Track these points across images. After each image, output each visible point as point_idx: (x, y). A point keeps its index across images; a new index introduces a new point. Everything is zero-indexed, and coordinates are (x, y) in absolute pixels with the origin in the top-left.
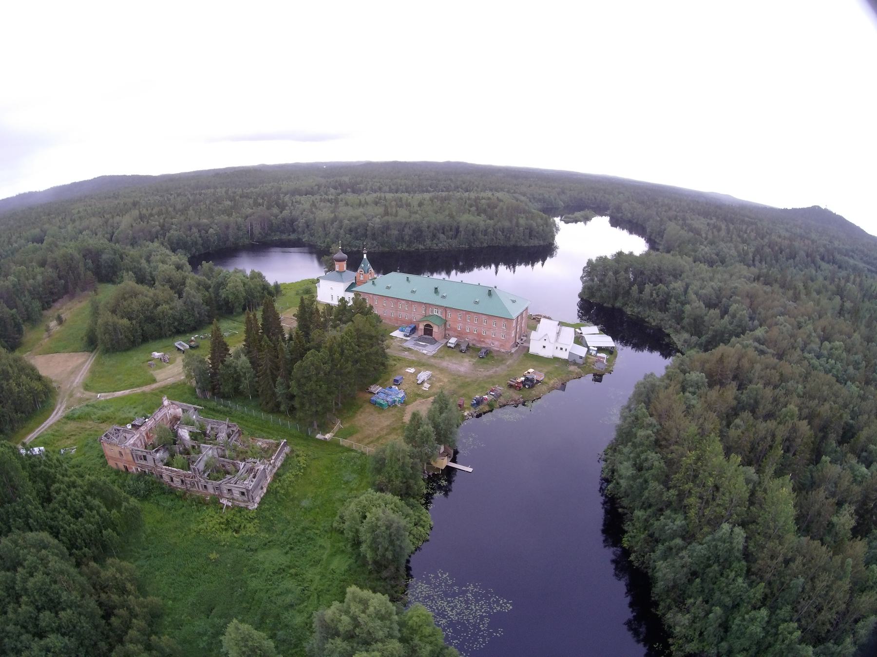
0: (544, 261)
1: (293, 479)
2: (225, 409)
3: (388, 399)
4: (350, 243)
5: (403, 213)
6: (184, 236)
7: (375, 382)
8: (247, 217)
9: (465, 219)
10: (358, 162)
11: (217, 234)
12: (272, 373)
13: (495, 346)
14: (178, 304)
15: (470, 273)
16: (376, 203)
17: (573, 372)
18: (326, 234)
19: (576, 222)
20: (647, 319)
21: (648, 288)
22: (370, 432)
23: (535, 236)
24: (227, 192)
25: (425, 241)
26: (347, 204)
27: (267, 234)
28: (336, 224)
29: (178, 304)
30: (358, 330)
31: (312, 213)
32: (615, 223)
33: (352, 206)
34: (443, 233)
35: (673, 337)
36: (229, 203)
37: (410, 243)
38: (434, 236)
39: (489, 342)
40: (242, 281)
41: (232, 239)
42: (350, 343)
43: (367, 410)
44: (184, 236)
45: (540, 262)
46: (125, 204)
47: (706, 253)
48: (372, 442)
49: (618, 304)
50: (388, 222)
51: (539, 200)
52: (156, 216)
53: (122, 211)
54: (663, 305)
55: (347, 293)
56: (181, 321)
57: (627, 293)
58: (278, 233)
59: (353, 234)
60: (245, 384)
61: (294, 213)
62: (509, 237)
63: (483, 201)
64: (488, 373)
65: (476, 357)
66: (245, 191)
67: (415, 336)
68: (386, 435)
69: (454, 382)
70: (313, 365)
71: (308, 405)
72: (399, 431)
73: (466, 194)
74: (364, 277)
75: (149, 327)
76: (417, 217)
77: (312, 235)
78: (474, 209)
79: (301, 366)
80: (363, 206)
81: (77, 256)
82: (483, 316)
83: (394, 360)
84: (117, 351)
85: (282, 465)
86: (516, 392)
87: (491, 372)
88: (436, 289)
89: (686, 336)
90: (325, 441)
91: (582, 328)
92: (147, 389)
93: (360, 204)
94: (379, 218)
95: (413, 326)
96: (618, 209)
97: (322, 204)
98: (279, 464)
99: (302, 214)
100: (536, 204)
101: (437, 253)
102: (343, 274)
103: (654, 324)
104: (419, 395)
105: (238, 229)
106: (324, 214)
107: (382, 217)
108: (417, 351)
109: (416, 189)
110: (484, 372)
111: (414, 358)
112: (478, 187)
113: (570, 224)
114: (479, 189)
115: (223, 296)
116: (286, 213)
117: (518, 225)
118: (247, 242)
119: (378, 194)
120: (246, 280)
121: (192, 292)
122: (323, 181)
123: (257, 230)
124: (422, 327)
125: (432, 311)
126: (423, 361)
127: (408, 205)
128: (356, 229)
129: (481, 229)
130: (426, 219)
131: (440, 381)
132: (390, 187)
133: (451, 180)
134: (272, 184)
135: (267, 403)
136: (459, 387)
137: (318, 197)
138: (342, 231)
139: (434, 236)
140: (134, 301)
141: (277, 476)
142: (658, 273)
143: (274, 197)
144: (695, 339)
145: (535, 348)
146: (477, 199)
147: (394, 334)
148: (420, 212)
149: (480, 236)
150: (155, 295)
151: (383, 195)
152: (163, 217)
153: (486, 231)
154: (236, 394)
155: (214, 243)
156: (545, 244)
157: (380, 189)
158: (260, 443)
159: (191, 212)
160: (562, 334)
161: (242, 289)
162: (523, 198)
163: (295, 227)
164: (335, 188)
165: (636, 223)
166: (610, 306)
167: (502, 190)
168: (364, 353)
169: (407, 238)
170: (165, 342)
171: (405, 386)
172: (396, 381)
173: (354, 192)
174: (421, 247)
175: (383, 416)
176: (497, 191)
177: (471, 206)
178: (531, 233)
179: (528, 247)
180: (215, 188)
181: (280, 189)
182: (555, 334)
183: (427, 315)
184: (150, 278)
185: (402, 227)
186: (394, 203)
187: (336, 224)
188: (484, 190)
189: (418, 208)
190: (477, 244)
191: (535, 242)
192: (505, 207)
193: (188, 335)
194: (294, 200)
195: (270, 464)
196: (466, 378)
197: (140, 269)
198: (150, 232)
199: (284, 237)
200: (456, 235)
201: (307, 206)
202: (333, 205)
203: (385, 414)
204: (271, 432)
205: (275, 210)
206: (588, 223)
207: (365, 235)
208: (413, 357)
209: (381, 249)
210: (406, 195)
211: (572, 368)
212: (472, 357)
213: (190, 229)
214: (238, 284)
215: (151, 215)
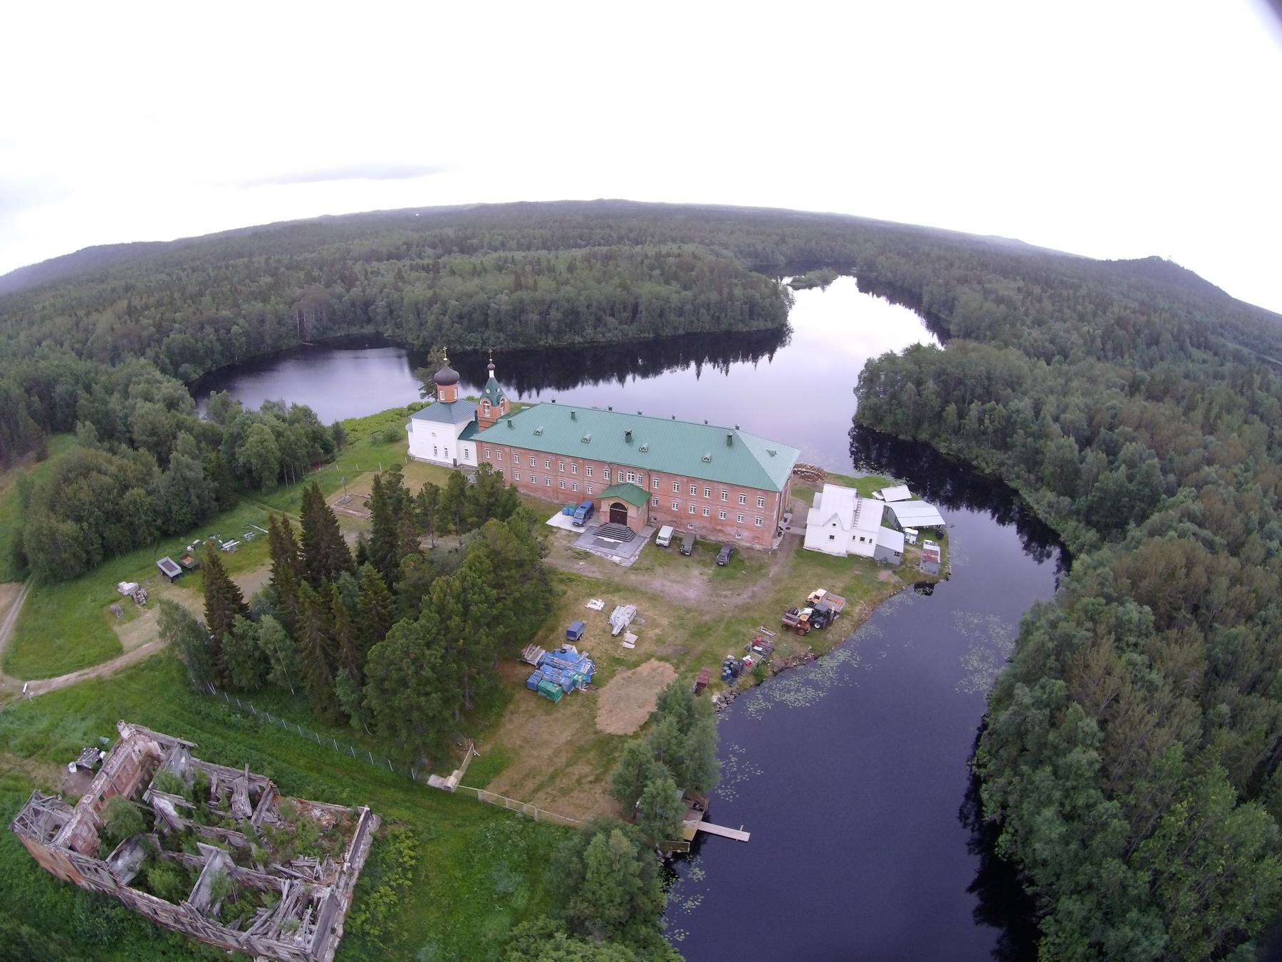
1: (394, 898)
3: (563, 681)
4: (460, 337)
5: (545, 283)
6: (192, 340)
7: (530, 639)
8: (293, 301)
9: (647, 290)
11: (246, 334)
12: (326, 654)
13: (743, 539)
14: (160, 479)
18: (421, 325)
19: (810, 287)
20: (975, 463)
23: (759, 314)
24: (267, 262)
25: (583, 329)
26: (453, 272)
27: (326, 328)
29: (160, 479)
30: (493, 554)
31: (397, 289)
32: (866, 285)
33: (461, 275)
34: (612, 315)
35: (1026, 496)
36: (268, 279)
38: (599, 320)
39: (733, 533)
40: (273, 429)
41: (269, 341)
42: (481, 588)
43: (523, 707)
44: (192, 340)
45: (766, 357)
46: (113, 290)
48: (540, 787)
49: (924, 436)
50: (521, 301)
51: (749, 255)
52: (153, 309)
53: (100, 304)
57: (939, 416)
59: (465, 322)
61: (368, 291)
62: (719, 317)
63: (671, 260)
64: (739, 600)
65: (711, 564)
66: (295, 257)
70: (407, 654)
71: (404, 733)
74: (492, 414)
75: (113, 532)
76: (568, 290)
78: (657, 272)
80: (479, 275)
81: (16, 391)
82: (721, 486)
83: (562, 581)
84: (62, 580)
85: (367, 864)
86: (800, 638)
87: (744, 598)
88: (628, 434)
89: (1050, 496)
90: (445, 793)
91: (884, 491)
92: (105, 670)
93: (475, 272)
94: (507, 295)
96: (871, 266)
97: (414, 274)
99: (381, 292)
100: (744, 260)
103: (987, 471)
104: (618, 661)
105: (279, 323)
106: (417, 291)
107: (512, 293)
108: (601, 558)
109: (559, 243)
110: (734, 598)
111: (598, 575)
112: (653, 236)
115: (241, 460)
116: (356, 291)
117: (731, 297)
119: (501, 254)
120: (283, 426)
121: (186, 459)
122: (415, 236)
124: (605, 507)
125: (623, 477)
127: (551, 270)
128: (470, 314)
131: (654, 624)
133: (610, 227)
134: (336, 245)
135: (325, 709)
136: (693, 635)
137: (407, 262)
139: (599, 320)
140: (83, 483)
141: (360, 894)
144: (1065, 501)
145: (815, 539)
146: (659, 256)
149: (673, 317)
150: (121, 468)
151: (509, 255)
152: (162, 309)
154: (261, 688)
156: (775, 326)
158: (317, 813)
159: (207, 299)
160: (862, 512)
161: (273, 445)
162: (725, 252)
164: (434, 247)
165: (901, 287)
166: (909, 438)
167: (692, 240)
168: (509, 602)
169: (554, 325)
170: (144, 556)
171: (587, 643)
173: (462, 251)
174: (578, 339)
175: (556, 720)
176: (683, 241)
177: (652, 268)
178: (753, 310)
179: (749, 333)
180: (251, 254)
181: (349, 252)
182: (851, 514)
184: (124, 429)
186: (528, 268)
188: (663, 241)
190: (667, 332)
191: (759, 324)
192: (706, 269)
194: (369, 270)
195: (342, 872)
197: (107, 413)
198: (140, 337)
200: (634, 317)
201: (389, 278)
202: (431, 275)
205: (339, 288)
206: (828, 288)
208: (594, 573)
209: (513, 345)
210: (544, 253)
211: (884, 575)
212: (705, 564)
213: (202, 327)
215: (147, 307)
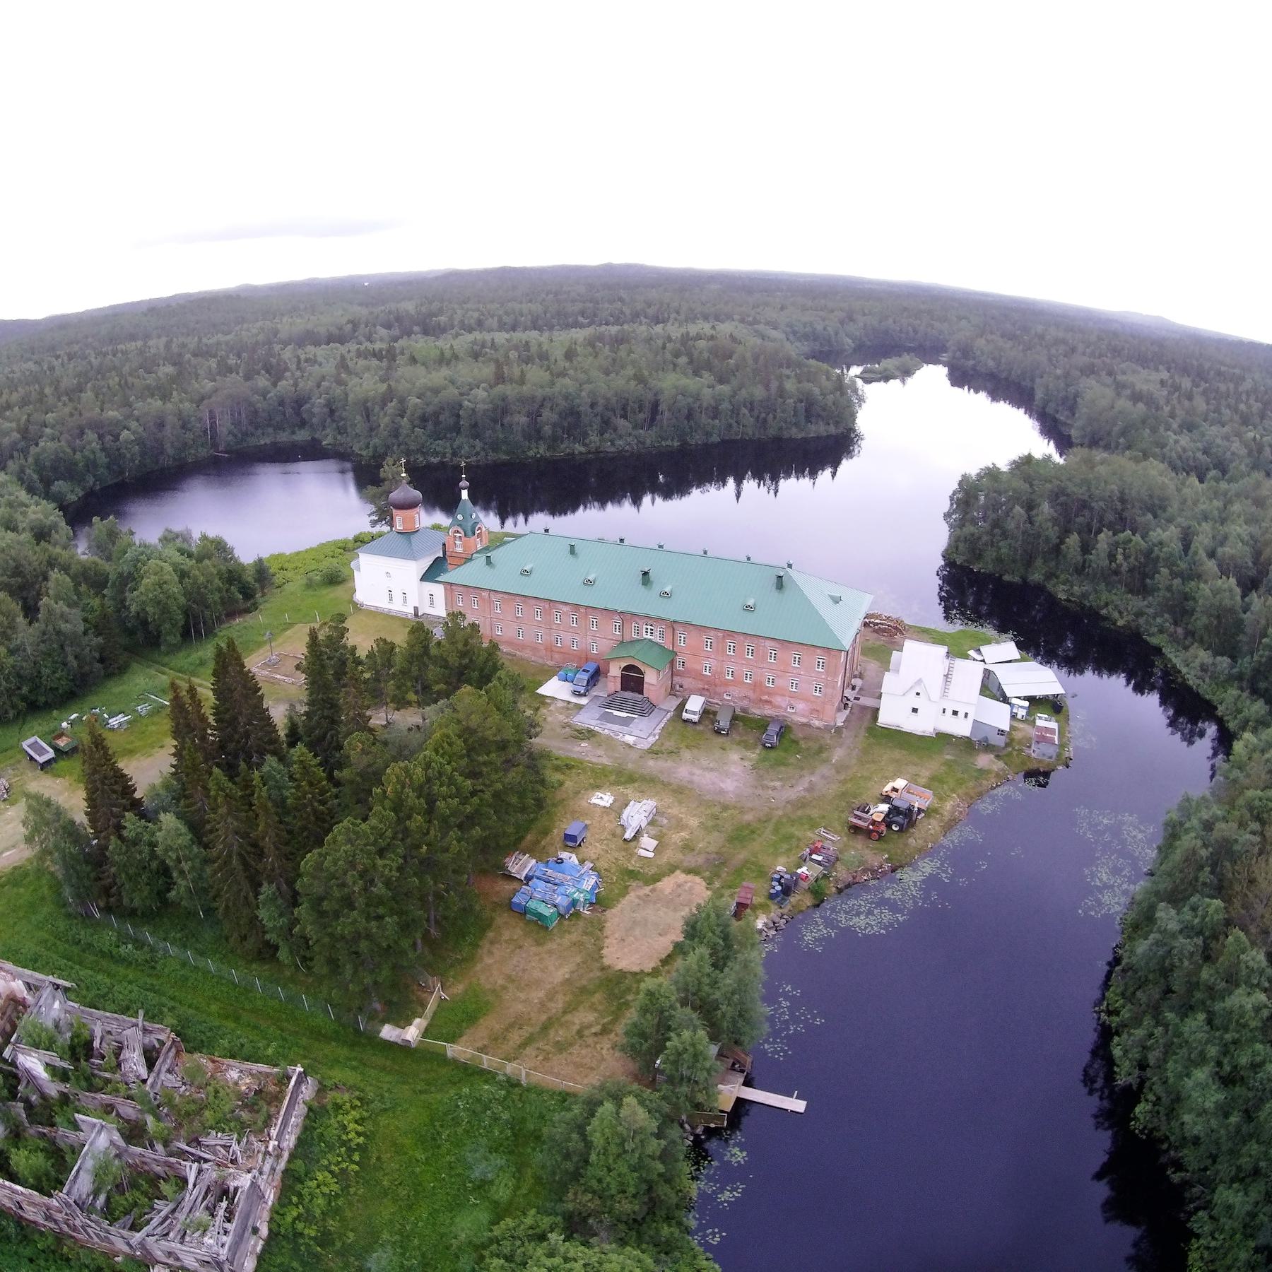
0: (835, 465)
1: (336, 1188)
2: (140, 956)
5: (536, 374)
7: (515, 845)
9: (670, 383)
10: (431, 272)
11: (140, 441)
12: (246, 865)
13: (798, 713)
15: (685, 499)
16: (476, 356)
17: (988, 772)
18: (371, 429)
19: (886, 379)
20: (1104, 612)
21: (1104, 539)
22: (520, 1007)
25: (585, 435)
26: (413, 360)
27: (246, 434)
28: (392, 406)
30: (467, 733)
31: (340, 382)
32: (960, 378)
33: (423, 364)
34: (624, 416)
35: (1171, 656)
37: (555, 440)
40: (176, 569)
43: (506, 935)
45: (828, 471)
47: (1184, 450)
49: (1036, 577)
51: (806, 337)
54: (1140, 581)
55: (425, 584)
56: (35, 681)
58: (270, 430)
59: (430, 426)
60: (181, 888)
62: (765, 420)
63: (702, 344)
65: (755, 747)
67: (599, 691)
68: (565, 1012)
69: (716, 827)
70: (352, 865)
71: (348, 970)
72: (598, 997)
73: (659, 328)
77: (341, 431)
78: (683, 360)
79: (319, 867)
82: (768, 643)
83: (557, 769)
85: (300, 1142)
86: (872, 844)
87: (798, 791)
88: (646, 574)
89: (1204, 656)
90: (403, 1049)
91: (983, 649)
93: (443, 360)
95: (591, 667)
96: (966, 351)
97: (362, 362)
98: (290, 1141)
99: (319, 386)
100: (798, 344)
101: (612, 459)
102: (414, 538)
103: (1120, 623)
104: (633, 875)
105: (183, 427)
106: (366, 384)
107: (491, 387)
108: (609, 738)
109: (555, 321)
111: (605, 761)
112: (678, 313)
113: (874, 384)
114: (682, 317)
115: (133, 608)
116: (285, 385)
117: (782, 392)
118: (203, 452)
119: (477, 335)
123: (225, 427)
124: (615, 671)
126: (630, 766)
127: (544, 356)
128: (436, 414)
129: (705, 405)
130: (587, 387)
131: (680, 826)
132: (500, 321)
136: (731, 840)
137: (353, 347)
138: (405, 422)
142: (1119, 506)
143: (261, 352)
144: (1224, 662)
145: (892, 714)
147: (545, 690)
148: (571, 372)
149: (704, 419)
151: (488, 337)
153: (716, 408)
155: (133, 460)
157: (480, 324)
160: (955, 677)
161: (175, 589)
162: (774, 334)
163: (305, 416)
164: (388, 326)
165: (1006, 379)
166: (1017, 579)
167: (729, 317)
169: (547, 430)
171: (591, 850)
172: (570, 838)
173: (426, 332)
174: (579, 448)
175: (550, 952)
177: (677, 355)
178: (810, 410)
179: (805, 440)
183: (627, 639)
185: (535, 408)
186: (513, 355)
187: (392, 406)
188: (692, 318)
189: (567, 365)
190: (697, 439)
191: (818, 429)
192: (748, 355)
193: (55, 713)
194: (303, 357)
196: (742, 811)
199: (284, 437)
201: (329, 368)
203: (551, 946)
204: (263, 1024)
205: (262, 381)
206: (909, 381)
207: (457, 429)
208: (598, 757)
209: (492, 456)
211: (984, 761)
212: (747, 747)
214: (167, 577)
